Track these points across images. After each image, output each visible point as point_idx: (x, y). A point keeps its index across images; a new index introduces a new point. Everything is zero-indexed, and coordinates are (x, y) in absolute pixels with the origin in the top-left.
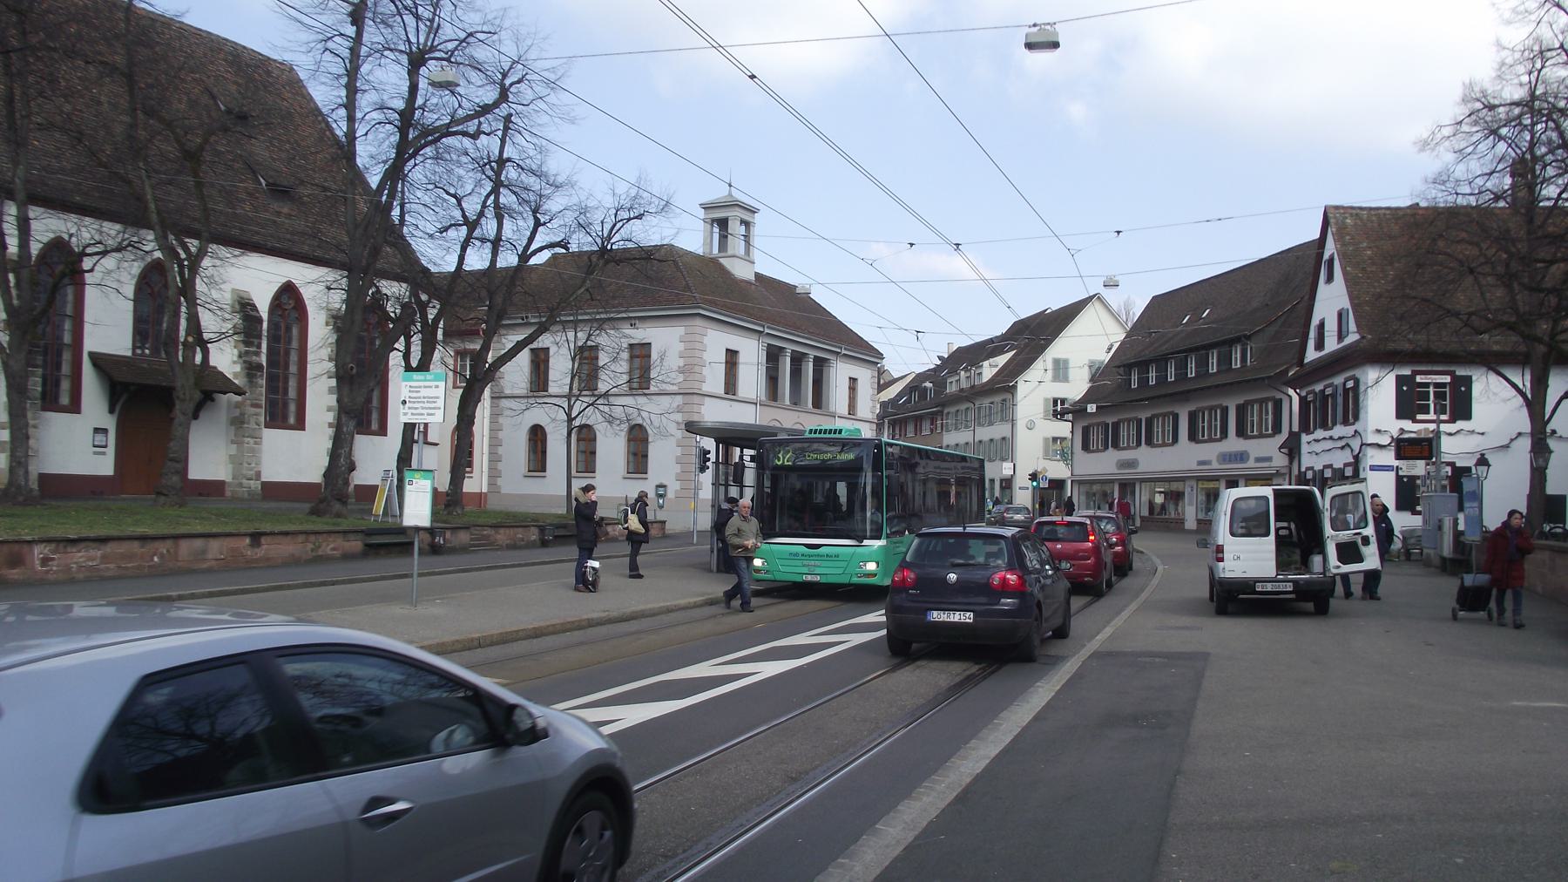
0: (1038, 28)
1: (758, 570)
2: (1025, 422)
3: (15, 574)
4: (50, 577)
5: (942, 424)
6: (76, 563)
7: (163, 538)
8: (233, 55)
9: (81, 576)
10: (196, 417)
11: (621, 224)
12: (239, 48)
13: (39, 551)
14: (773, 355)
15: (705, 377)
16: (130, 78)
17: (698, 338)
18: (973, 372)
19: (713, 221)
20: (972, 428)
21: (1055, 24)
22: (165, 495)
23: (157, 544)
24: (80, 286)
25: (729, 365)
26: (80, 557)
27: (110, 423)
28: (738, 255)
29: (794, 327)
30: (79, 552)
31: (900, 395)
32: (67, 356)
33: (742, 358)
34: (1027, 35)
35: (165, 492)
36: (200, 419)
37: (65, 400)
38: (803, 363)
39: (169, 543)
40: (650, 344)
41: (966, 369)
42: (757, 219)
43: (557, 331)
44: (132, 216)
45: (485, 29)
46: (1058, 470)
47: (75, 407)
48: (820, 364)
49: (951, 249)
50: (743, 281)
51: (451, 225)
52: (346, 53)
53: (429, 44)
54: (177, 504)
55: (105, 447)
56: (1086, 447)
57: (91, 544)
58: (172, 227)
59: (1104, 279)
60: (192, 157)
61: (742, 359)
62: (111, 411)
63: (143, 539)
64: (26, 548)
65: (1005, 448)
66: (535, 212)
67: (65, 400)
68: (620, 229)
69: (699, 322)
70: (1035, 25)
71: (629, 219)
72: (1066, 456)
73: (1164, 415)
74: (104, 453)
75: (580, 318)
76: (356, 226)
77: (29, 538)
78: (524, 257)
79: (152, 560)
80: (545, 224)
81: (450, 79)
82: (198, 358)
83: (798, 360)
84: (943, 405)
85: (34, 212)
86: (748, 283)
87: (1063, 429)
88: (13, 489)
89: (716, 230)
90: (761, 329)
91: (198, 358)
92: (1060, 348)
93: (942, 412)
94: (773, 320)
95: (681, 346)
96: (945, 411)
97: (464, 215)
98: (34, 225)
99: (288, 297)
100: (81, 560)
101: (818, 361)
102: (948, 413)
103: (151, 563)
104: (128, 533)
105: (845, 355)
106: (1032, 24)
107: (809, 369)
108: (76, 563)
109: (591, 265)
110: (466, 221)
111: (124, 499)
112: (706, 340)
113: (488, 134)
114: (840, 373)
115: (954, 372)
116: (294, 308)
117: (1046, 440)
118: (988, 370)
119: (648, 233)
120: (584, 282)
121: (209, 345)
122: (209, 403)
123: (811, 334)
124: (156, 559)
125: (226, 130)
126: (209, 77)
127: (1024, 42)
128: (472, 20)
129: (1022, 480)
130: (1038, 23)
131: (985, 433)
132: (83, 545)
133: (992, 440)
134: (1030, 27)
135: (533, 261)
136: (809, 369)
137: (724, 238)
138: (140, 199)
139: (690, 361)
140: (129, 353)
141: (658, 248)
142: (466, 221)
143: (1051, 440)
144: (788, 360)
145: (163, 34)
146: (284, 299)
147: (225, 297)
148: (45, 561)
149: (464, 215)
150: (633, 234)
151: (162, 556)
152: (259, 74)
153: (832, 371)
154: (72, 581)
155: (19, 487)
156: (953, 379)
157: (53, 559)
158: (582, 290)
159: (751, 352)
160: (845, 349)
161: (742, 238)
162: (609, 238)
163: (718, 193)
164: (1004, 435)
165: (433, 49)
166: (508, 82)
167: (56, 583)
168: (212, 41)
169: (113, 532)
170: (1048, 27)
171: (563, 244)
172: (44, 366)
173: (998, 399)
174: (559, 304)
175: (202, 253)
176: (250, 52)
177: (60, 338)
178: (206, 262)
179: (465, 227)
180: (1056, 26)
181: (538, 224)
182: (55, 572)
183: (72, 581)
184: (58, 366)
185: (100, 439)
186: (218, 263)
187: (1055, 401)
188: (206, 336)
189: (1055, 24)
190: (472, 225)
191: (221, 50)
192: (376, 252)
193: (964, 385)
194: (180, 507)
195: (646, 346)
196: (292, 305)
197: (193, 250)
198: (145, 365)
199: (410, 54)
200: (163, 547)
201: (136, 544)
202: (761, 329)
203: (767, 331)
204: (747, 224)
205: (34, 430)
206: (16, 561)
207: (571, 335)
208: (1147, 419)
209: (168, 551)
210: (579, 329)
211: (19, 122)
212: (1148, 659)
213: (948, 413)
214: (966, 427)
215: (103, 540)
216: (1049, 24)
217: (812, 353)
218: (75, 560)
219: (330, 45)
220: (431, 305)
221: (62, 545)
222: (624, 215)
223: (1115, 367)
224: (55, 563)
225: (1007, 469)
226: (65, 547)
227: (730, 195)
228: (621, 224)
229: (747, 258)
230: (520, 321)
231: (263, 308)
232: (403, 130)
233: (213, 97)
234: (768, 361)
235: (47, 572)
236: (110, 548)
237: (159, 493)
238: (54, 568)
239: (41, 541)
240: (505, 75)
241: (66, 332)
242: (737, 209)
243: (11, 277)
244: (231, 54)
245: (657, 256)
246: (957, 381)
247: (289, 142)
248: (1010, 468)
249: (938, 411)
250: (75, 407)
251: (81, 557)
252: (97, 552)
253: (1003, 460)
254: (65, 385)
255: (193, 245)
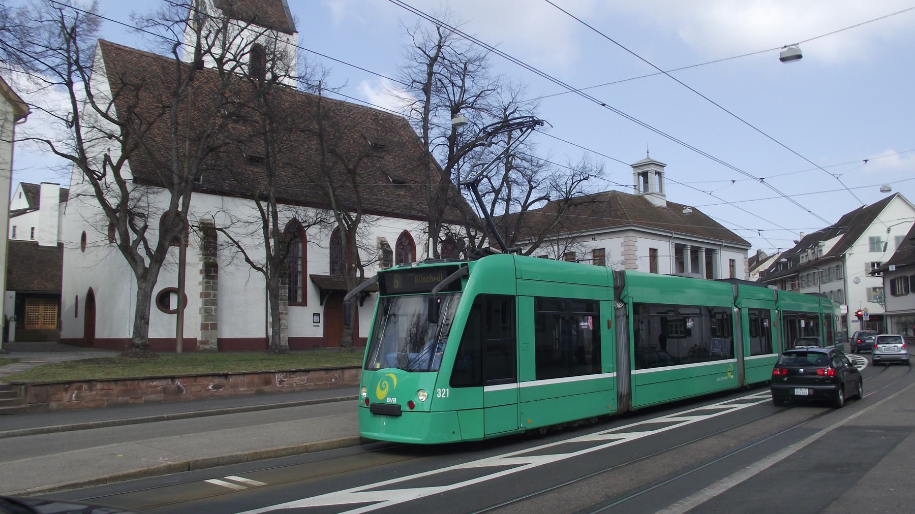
0: (787, 48)
1: (801, 374)
2: (853, 279)
3: (267, 388)
4: (284, 390)
5: (799, 283)
6: (295, 383)
7: (337, 369)
8: (375, 116)
9: (297, 389)
10: (362, 305)
11: (576, 183)
12: (377, 111)
13: (278, 377)
14: (679, 250)
15: (637, 265)
16: (320, 136)
17: (632, 243)
18: (816, 249)
19: (639, 174)
20: (818, 285)
21: (798, 44)
22: (344, 347)
23: (333, 372)
24: (305, 242)
25: (652, 258)
26: (297, 379)
27: (320, 310)
28: (655, 192)
29: (693, 232)
30: (297, 377)
31: (771, 267)
32: (300, 277)
33: (660, 253)
34: (781, 54)
35: (344, 345)
36: (364, 305)
37: (300, 300)
38: (699, 253)
39: (339, 372)
40: (604, 249)
41: (812, 249)
42: (666, 171)
43: (548, 246)
44: (322, 204)
45: (489, 88)
46: (876, 309)
47: (304, 303)
48: (710, 253)
49: (758, 182)
50: (659, 207)
51: (486, 193)
52: (422, 110)
53: (461, 100)
54: (350, 351)
55: (319, 322)
56: (894, 293)
57: (302, 373)
58: (343, 208)
59: (881, 187)
60: (352, 173)
61: (660, 253)
62: (321, 304)
63: (327, 370)
64: (272, 375)
65: (841, 296)
66: (529, 182)
67: (300, 300)
68: (575, 187)
69: (631, 234)
70: (785, 47)
71: (580, 181)
72: (882, 300)
73: (901, 278)
74: (318, 326)
75: (560, 237)
76: (432, 199)
77: (273, 371)
78: (525, 207)
79: (332, 381)
80: (535, 187)
81: (462, 121)
82: (358, 275)
83: (695, 252)
84: (799, 271)
85: (279, 207)
86: (663, 208)
87: (878, 281)
88: (274, 346)
89: (641, 178)
90: (670, 235)
91: (358, 275)
92: (875, 229)
93: (798, 276)
94: (677, 229)
95: (622, 249)
96: (800, 276)
97: (493, 187)
98: (279, 215)
99: (406, 239)
100: (297, 381)
101: (707, 250)
102: (802, 276)
103: (331, 382)
104: (320, 367)
105: (725, 246)
106: (784, 46)
107: (703, 256)
108: (295, 383)
109: (560, 209)
110: (494, 190)
111: (328, 349)
112: (637, 244)
113: (496, 144)
114: (723, 258)
115: (804, 251)
116: (408, 244)
117: (868, 289)
118: (828, 246)
119: (592, 187)
120: (557, 218)
121: (364, 268)
122: (368, 297)
123: (703, 235)
124: (333, 380)
125: (368, 156)
126: (363, 129)
127: (779, 57)
128: (484, 84)
129: (852, 317)
130: (787, 45)
131: (826, 288)
132: (298, 374)
133: (831, 292)
134: (782, 48)
135: (530, 208)
136: (703, 256)
137: (646, 182)
138: (327, 195)
139: (627, 257)
140: (329, 274)
141: (599, 194)
142: (494, 190)
143: (872, 289)
144: (689, 252)
145: (341, 110)
146: (404, 240)
147: (373, 242)
148: (281, 382)
149: (493, 187)
150: (583, 189)
151: (336, 379)
152: (388, 124)
153: (718, 257)
154: (294, 392)
155: (276, 345)
156: (804, 255)
157: (285, 381)
158: (556, 223)
159: (665, 249)
160: (725, 242)
161: (633, 187)
162: (570, 192)
163: (640, 158)
164: (839, 288)
165: (463, 103)
166: (507, 113)
167: (287, 393)
168: (364, 109)
169: (314, 367)
170: (794, 47)
171: (546, 197)
172: (290, 284)
173: (834, 265)
174: (544, 231)
175: (358, 221)
176: (383, 113)
177: (297, 268)
178: (360, 225)
179: (493, 193)
180: (798, 46)
181: (531, 188)
182: (285, 387)
183: (294, 392)
184: (296, 283)
185: (316, 318)
186: (366, 225)
187: (873, 265)
188: (362, 263)
189: (798, 44)
190: (497, 192)
191: (369, 114)
192: (441, 213)
193: (811, 258)
194: (352, 352)
195: (602, 250)
196: (408, 242)
197: (354, 219)
198: (336, 280)
199: (451, 107)
200: (336, 374)
201: (323, 373)
202: (671, 235)
203: (674, 236)
204: (659, 174)
205: (285, 315)
206: (268, 382)
207: (556, 247)
208: (910, 276)
209: (339, 376)
210: (559, 244)
211: (271, 165)
212: (872, 431)
213: (802, 276)
214: (814, 284)
215: (307, 371)
216: (794, 45)
217: (704, 247)
218: (295, 381)
219: (414, 106)
220: (477, 237)
221: (288, 374)
222: (577, 178)
223: (910, 240)
224: (286, 383)
225: (843, 310)
226: (290, 375)
227: (648, 158)
228: (576, 183)
229: (661, 194)
230: (528, 242)
231: (393, 246)
232: (451, 148)
233: (365, 139)
234: (676, 253)
235: (282, 387)
236: (311, 375)
237: (341, 346)
238: (285, 386)
239: (279, 372)
240: (506, 110)
241: (299, 266)
242: (652, 165)
243: (350, 223)
244: (374, 115)
245: (598, 199)
246: (806, 256)
247: (403, 157)
248: (845, 309)
249: (795, 276)
250: (304, 303)
251: (297, 380)
252: (305, 377)
253: (841, 304)
254: (300, 292)
255: (354, 215)
